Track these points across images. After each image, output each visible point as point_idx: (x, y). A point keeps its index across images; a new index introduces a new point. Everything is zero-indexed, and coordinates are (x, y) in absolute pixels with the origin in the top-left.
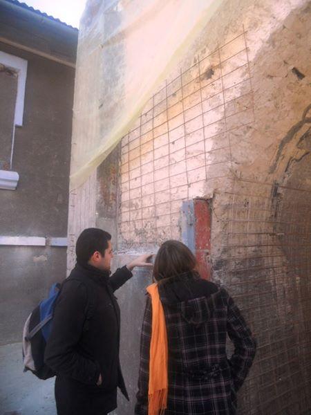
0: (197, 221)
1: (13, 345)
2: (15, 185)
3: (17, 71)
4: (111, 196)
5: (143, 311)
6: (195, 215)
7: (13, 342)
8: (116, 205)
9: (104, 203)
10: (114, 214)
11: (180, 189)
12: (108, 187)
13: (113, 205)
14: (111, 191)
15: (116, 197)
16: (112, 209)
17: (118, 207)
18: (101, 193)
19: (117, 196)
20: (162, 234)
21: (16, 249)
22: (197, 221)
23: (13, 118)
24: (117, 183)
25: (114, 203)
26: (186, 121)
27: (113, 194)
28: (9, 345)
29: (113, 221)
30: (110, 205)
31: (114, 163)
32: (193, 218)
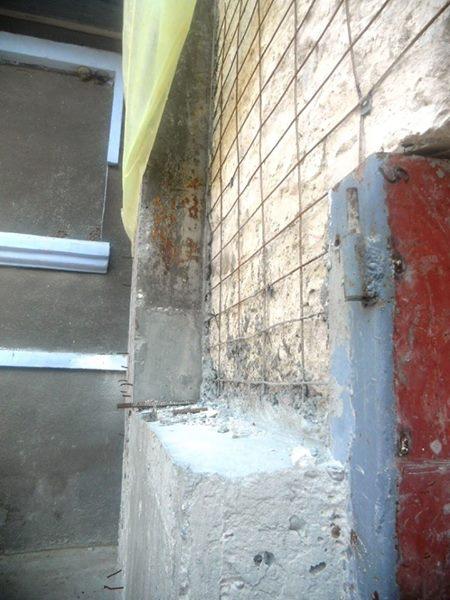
0: (409, 276)
1: (98, 549)
2: (105, 263)
3: (111, 76)
4: (184, 250)
5: (343, 129)
6: (393, 242)
7: (101, 544)
8: (199, 272)
9: (161, 267)
10: (193, 297)
11: (333, 146)
12: (175, 224)
13: (191, 273)
14: (186, 235)
15: (199, 250)
16: (187, 283)
17: (204, 276)
18: (152, 238)
19: (199, 248)
20: (283, 354)
21: (107, 377)
22: (409, 276)
23: (105, 153)
24: (201, 211)
25: (193, 265)
26: (303, 263)
27: (191, 244)
28: (90, 549)
29: (190, 317)
30: (183, 272)
31: (197, 162)
32: (382, 261)
